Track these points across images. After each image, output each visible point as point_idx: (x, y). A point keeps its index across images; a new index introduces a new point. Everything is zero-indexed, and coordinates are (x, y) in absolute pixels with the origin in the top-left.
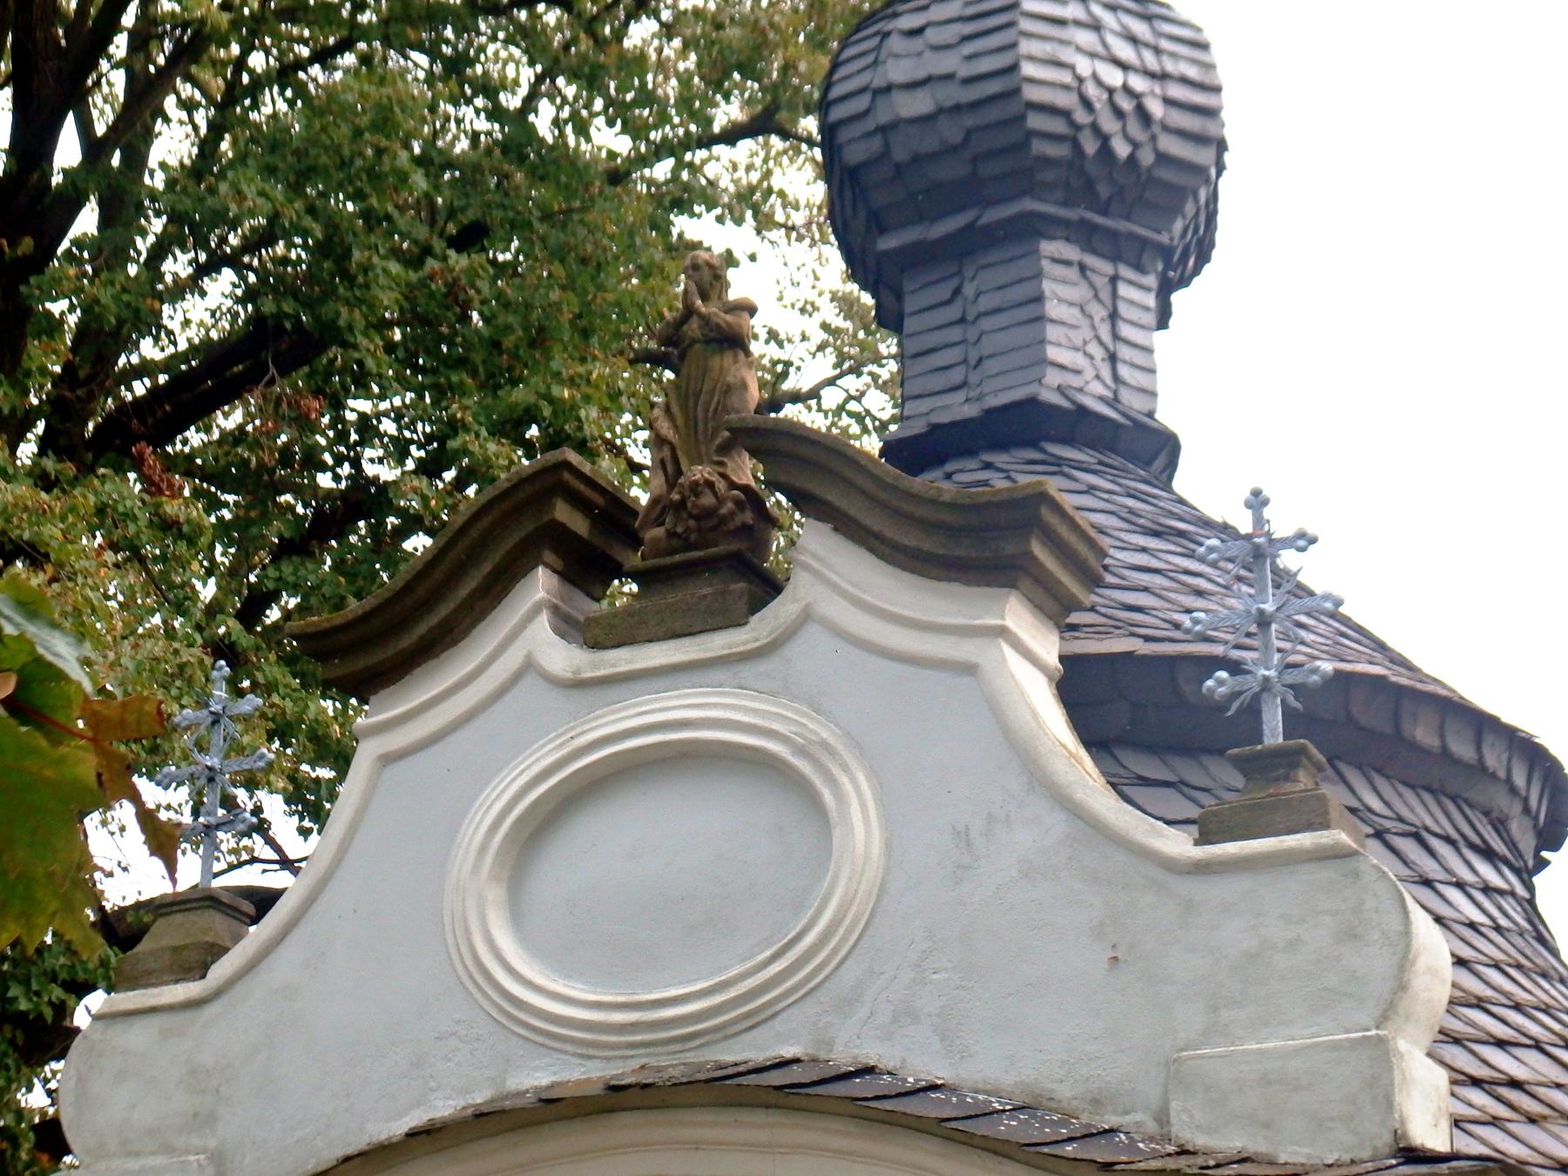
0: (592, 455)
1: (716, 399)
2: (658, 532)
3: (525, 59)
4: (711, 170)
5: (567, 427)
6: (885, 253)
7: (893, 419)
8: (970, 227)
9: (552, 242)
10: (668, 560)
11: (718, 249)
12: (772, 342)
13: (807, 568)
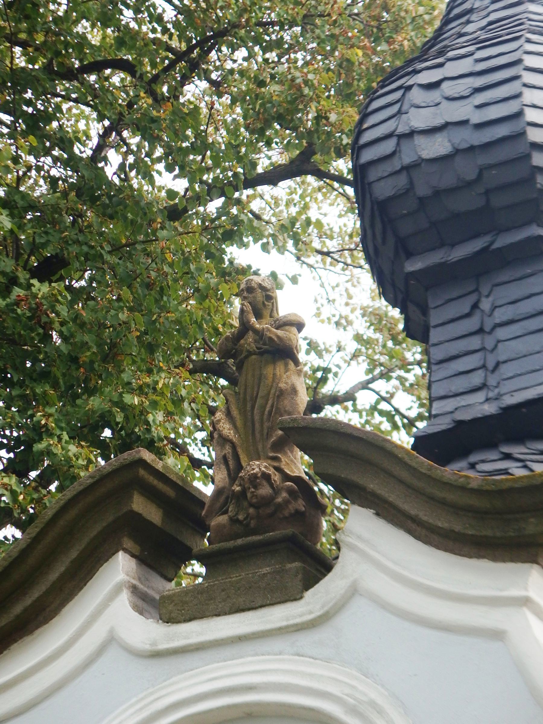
0: (160, 453)
1: (270, 402)
2: (223, 519)
3: (95, 115)
4: (256, 205)
5: (137, 430)
6: (412, 273)
7: (420, 417)
8: (485, 250)
9: (120, 270)
10: (231, 544)
11: (265, 272)
12: (313, 353)
13: (353, 548)
